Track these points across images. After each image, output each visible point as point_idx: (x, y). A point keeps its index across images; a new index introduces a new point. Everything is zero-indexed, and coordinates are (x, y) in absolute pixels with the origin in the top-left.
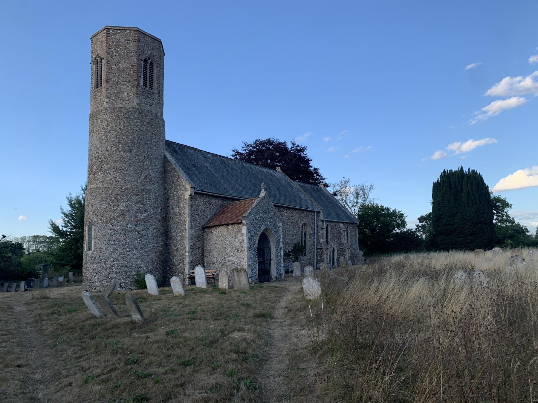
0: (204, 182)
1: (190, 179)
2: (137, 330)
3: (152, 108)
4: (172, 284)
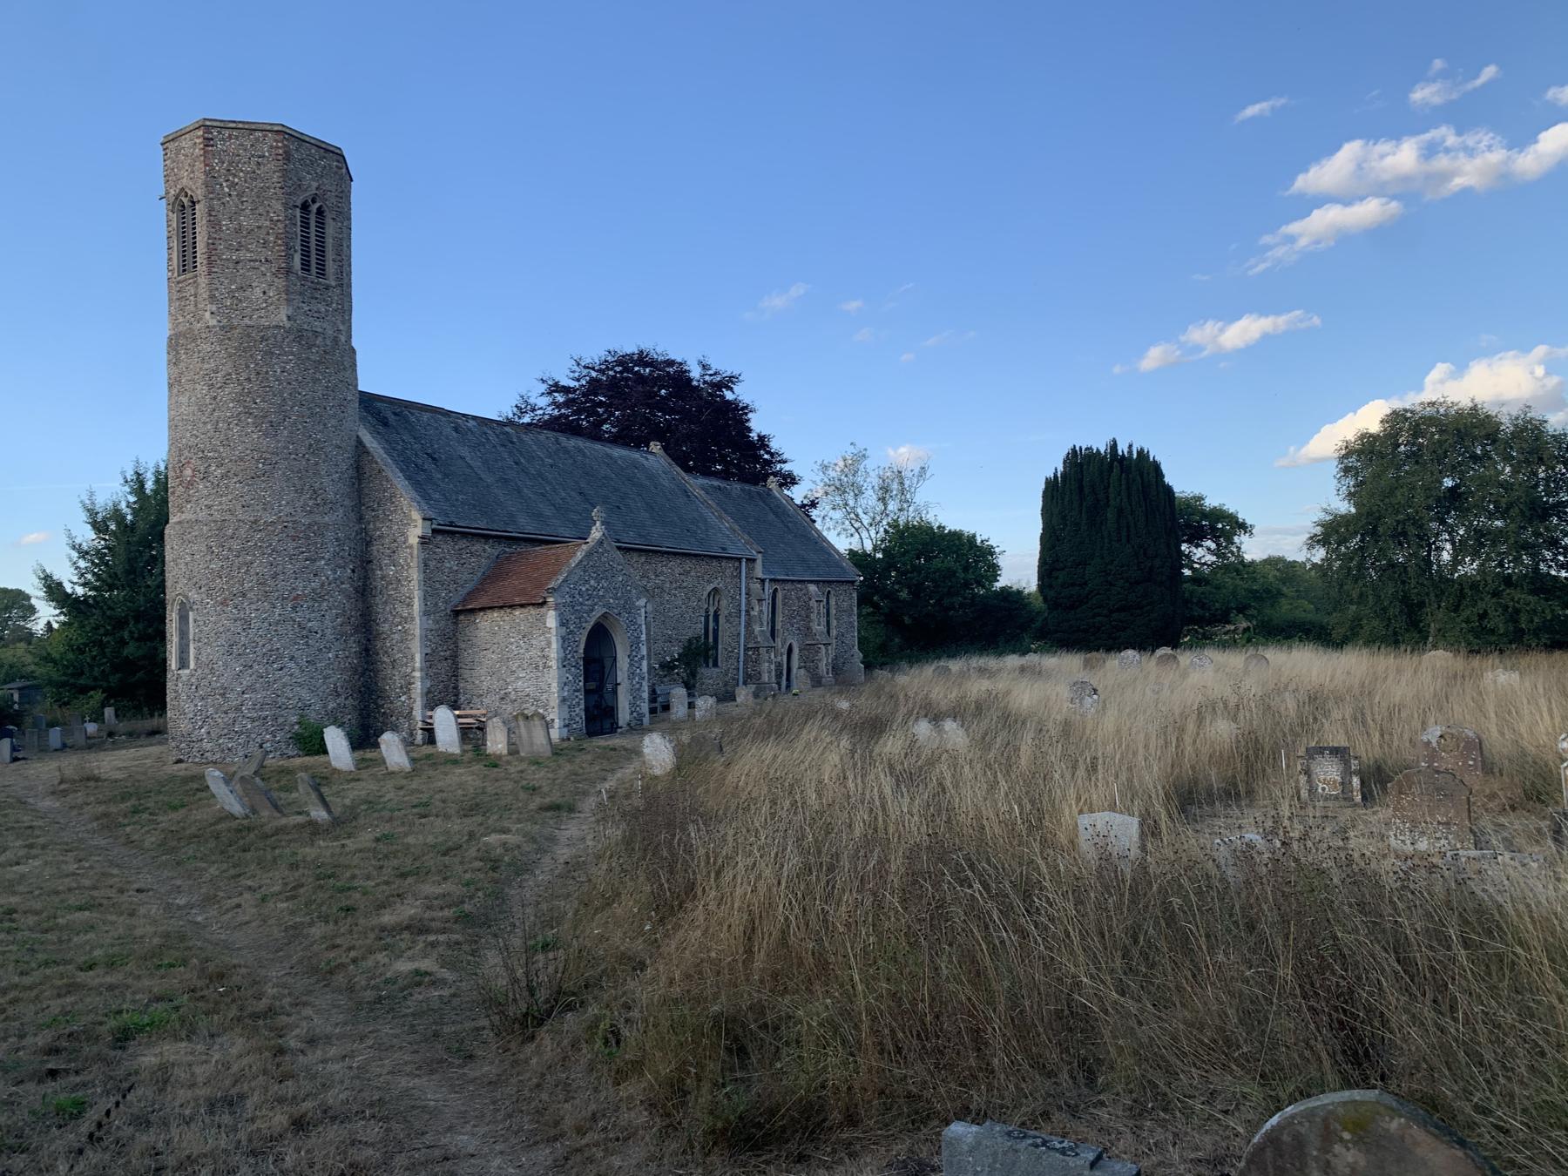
0: (457, 500)
1: (421, 496)
2: (321, 836)
3: (325, 326)
4: (383, 747)
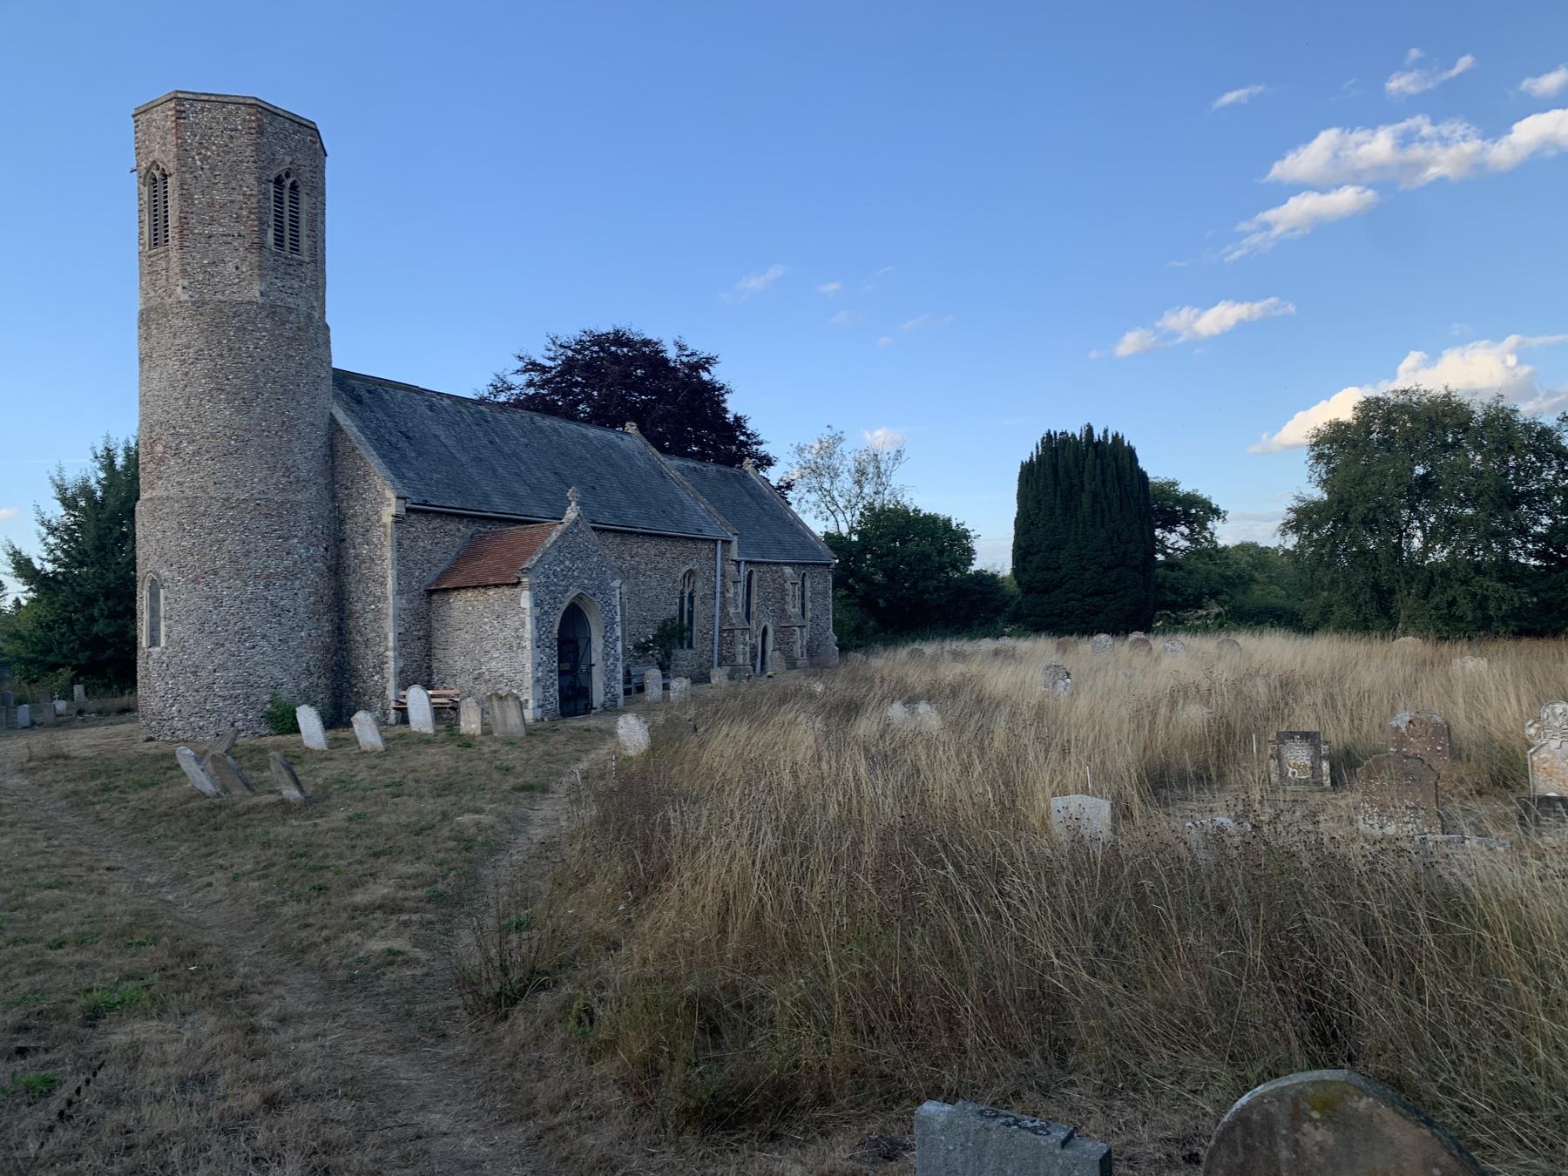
0: (431, 479)
3: (299, 301)
